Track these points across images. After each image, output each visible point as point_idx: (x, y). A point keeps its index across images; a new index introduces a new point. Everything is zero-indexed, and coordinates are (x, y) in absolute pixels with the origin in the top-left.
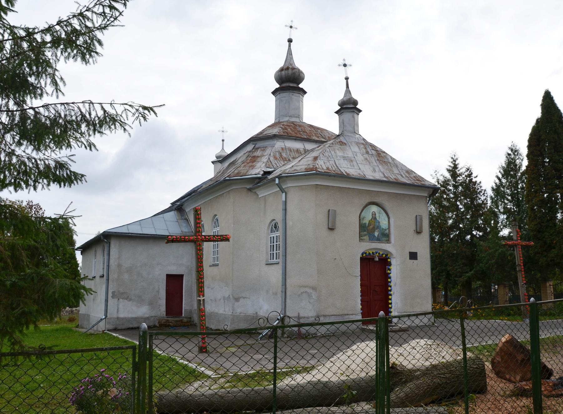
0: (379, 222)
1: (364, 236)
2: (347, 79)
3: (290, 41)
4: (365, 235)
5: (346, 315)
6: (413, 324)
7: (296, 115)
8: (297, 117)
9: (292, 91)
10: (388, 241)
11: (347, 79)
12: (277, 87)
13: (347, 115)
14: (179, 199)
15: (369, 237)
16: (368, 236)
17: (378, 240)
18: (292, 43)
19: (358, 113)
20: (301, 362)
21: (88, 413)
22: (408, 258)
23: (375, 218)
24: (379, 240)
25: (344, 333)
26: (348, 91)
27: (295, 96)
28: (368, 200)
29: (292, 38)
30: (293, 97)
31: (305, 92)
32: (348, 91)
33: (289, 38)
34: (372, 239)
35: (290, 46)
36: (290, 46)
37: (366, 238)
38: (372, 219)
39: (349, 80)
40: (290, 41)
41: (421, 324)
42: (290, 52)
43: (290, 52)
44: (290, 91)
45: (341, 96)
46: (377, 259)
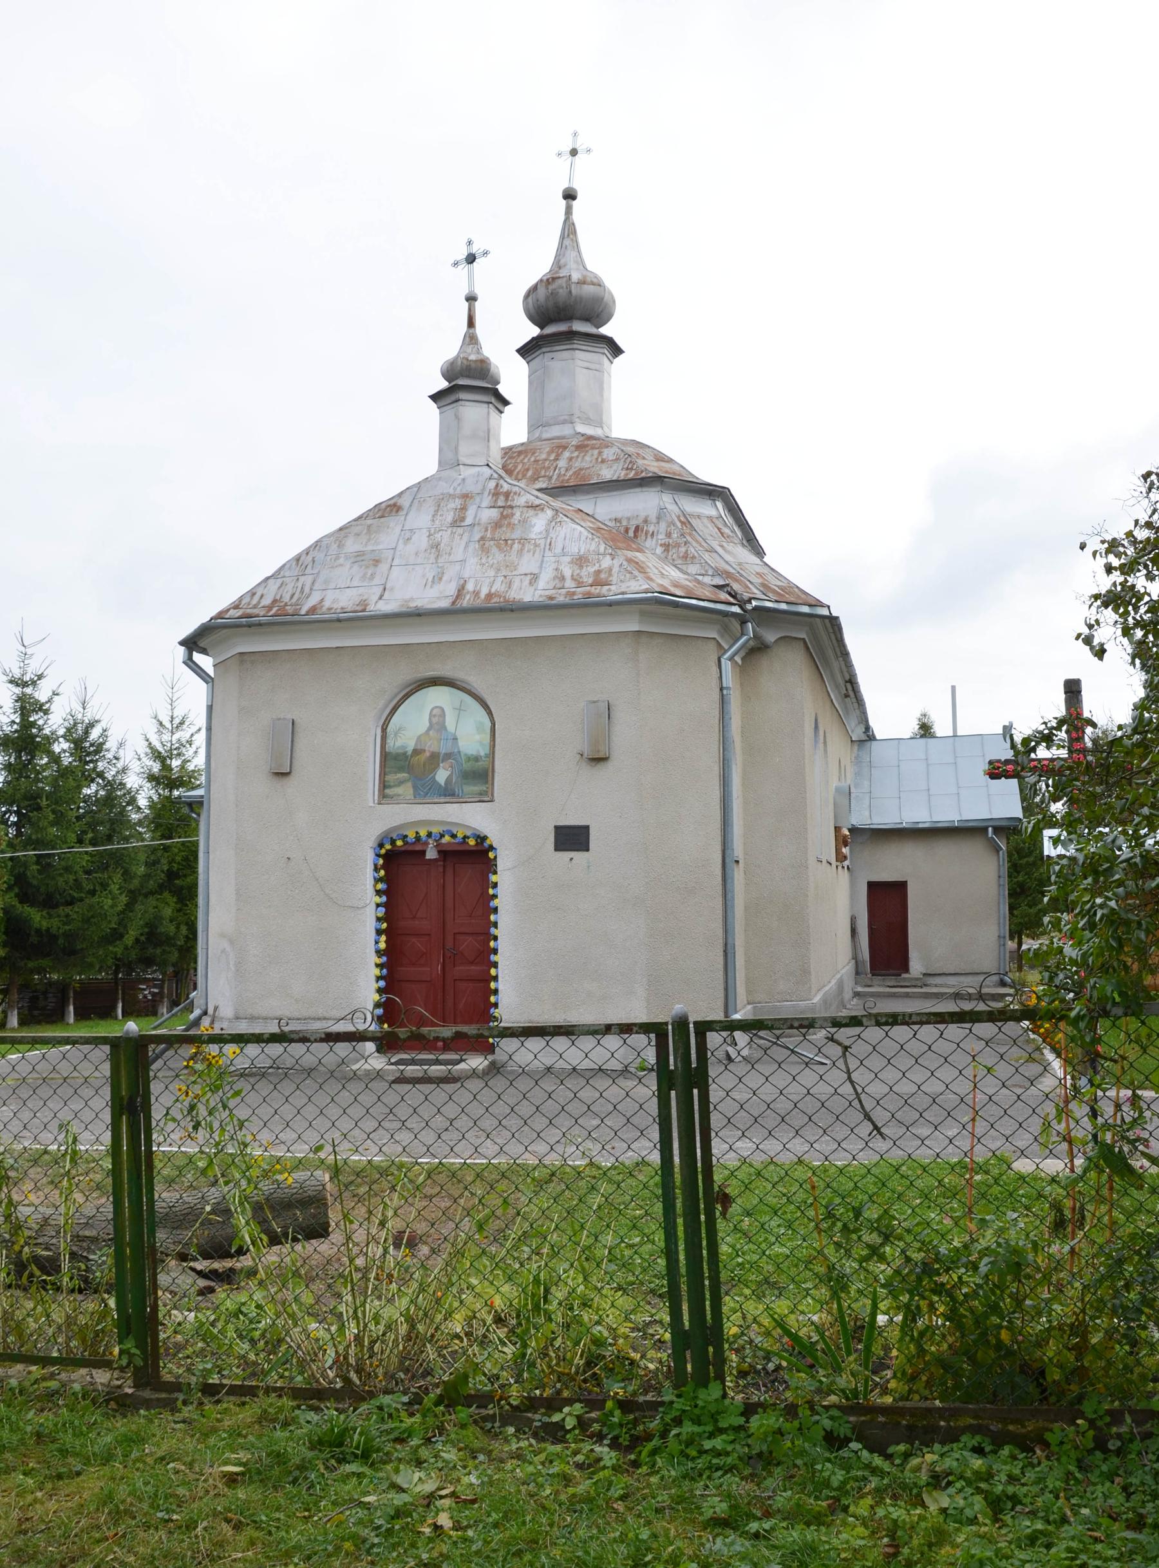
0: (455, 739)
1: (395, 786)
2: (471, 299)
3: (570, 196)
4: (401, 783)
5: (319, 1019)
6: (561, 1064)
7: (562, 418)
8: (564, 422)
9: (548, 349)
10: (486, 797)
11: (471, 299)
12: (535, 335)
13: (472, 411)
14: (852, 666)
15: (415, 787)
16: (409, 784)
17: (449, 793)
18: (575, 203)
19: (500, 406)
20: (739, 1144)
21: (5, 1241)
22: (585, 853)
23: (442, 727)
24: (453, 795)
25: (309, 1072)
26: (471, 339)
27: (581, 358)
28: (407, 672)
29: (575, 186)
30: (552, 364)
31: (616, 350)
32: (471, 339)
33: (566, 186)
34: (427, 791)
35: (569, 211)
36: (569, 211)
37: (406, 790)
38: (429, 729)
39: (477, 303)
40: (570, 196)
41: (586, 1065)
42: (569, 231)
43: (569, 231)
44: (544, 350)
45: (450, 348)
46: (431, 854)
